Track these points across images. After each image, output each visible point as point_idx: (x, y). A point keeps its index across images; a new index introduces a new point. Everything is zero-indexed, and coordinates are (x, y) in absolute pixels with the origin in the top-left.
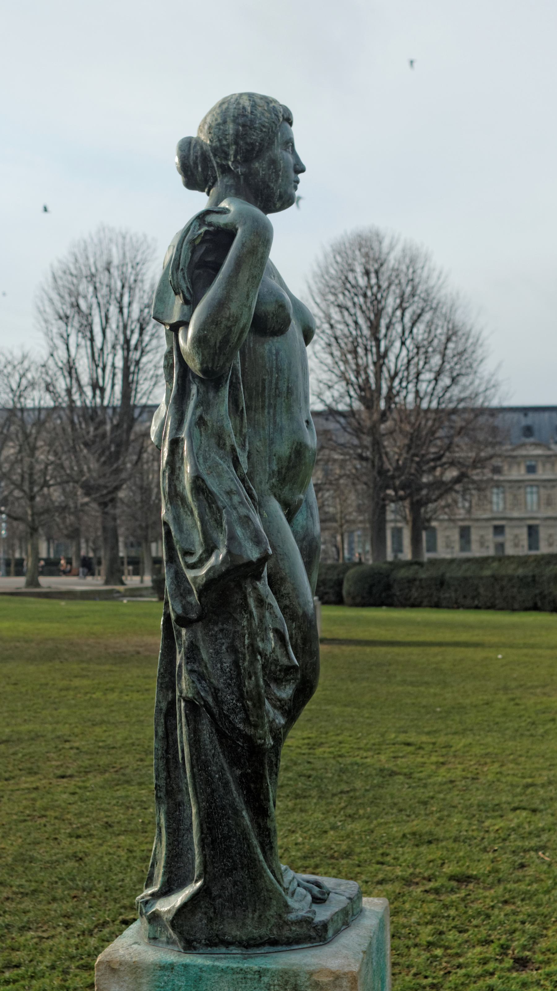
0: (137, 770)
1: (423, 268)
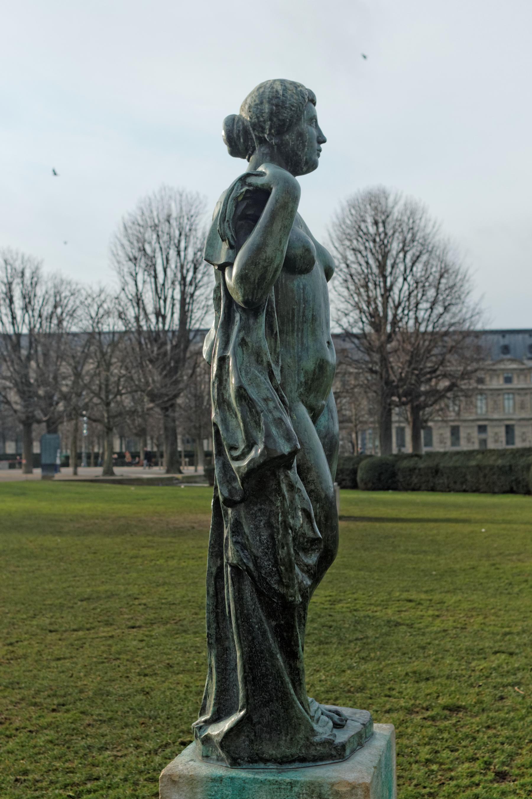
0: (192, 621)
1: (421, 219)
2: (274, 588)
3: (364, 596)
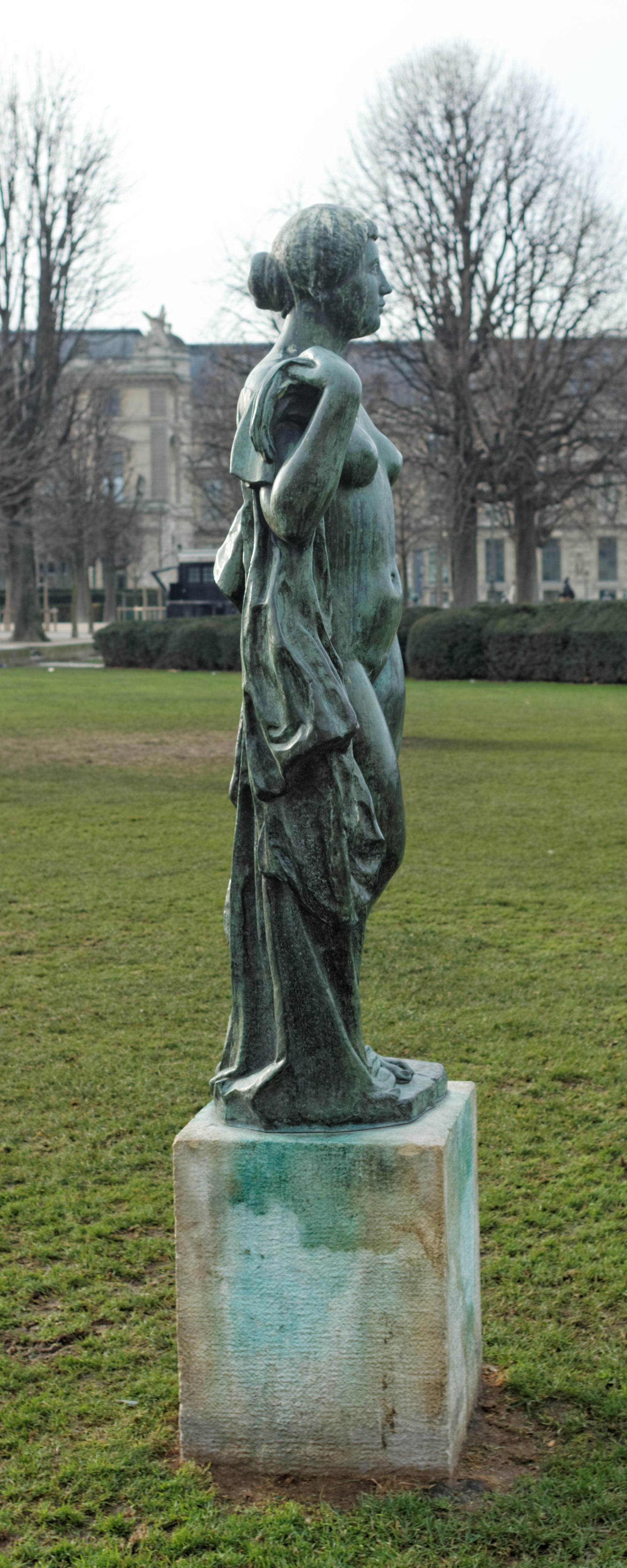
0: (122, 942)
1: (543, 109)
2: (323, 906)
3: (423, 896)
